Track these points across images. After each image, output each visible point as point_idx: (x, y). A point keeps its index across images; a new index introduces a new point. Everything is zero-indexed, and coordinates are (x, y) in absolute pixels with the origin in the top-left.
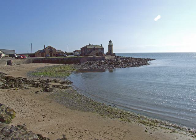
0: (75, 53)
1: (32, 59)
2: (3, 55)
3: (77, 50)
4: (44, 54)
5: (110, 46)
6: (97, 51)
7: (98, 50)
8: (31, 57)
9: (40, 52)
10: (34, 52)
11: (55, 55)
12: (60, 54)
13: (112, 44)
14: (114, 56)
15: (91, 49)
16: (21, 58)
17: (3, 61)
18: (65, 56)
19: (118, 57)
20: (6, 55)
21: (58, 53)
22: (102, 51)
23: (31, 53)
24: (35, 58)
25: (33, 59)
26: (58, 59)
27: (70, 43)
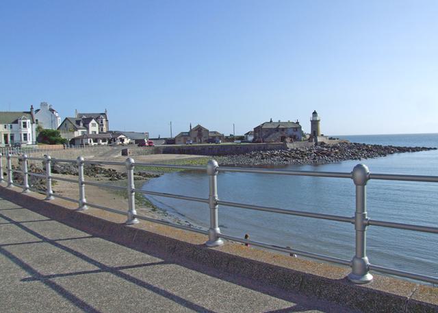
0: (247, 138)
2: (126, 141)
5: (315, 124)
6: (281, 133)
8: (168, 143)
12: (215, 137)
13: (318, 119)
20: (132, 141)
21: (214, 137)
24: (170, 146)
27: (235, 120)
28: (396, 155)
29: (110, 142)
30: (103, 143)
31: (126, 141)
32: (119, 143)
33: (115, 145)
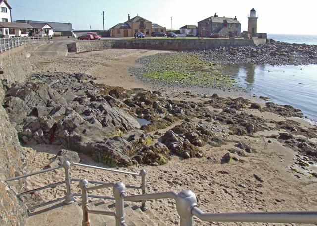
1: (110, 40)
2: (51, 33)
3: (189, 26)
4: (129, 31)
5: (252, 20)
7: (230, 25)
9: (121, 28)
10: (107, 28)
11: (150, 32)
12: (159, 31)
13: (256, 17)
14: (265, 40)
15: (219, 24)
16: (91, 39)
17: (60, 44)
18: (174, 36)
19: (272, 40)
20: (57, 33)
21: (156, 30)
22: (237, 29)
23: (102, 29)
25: (113, 40)
26: (162, 42)
28: (270, 135)
29: (30, 34)
30: (23, 35)
31: (51, 33)
32: (44, 35)
33: (40, 38)
